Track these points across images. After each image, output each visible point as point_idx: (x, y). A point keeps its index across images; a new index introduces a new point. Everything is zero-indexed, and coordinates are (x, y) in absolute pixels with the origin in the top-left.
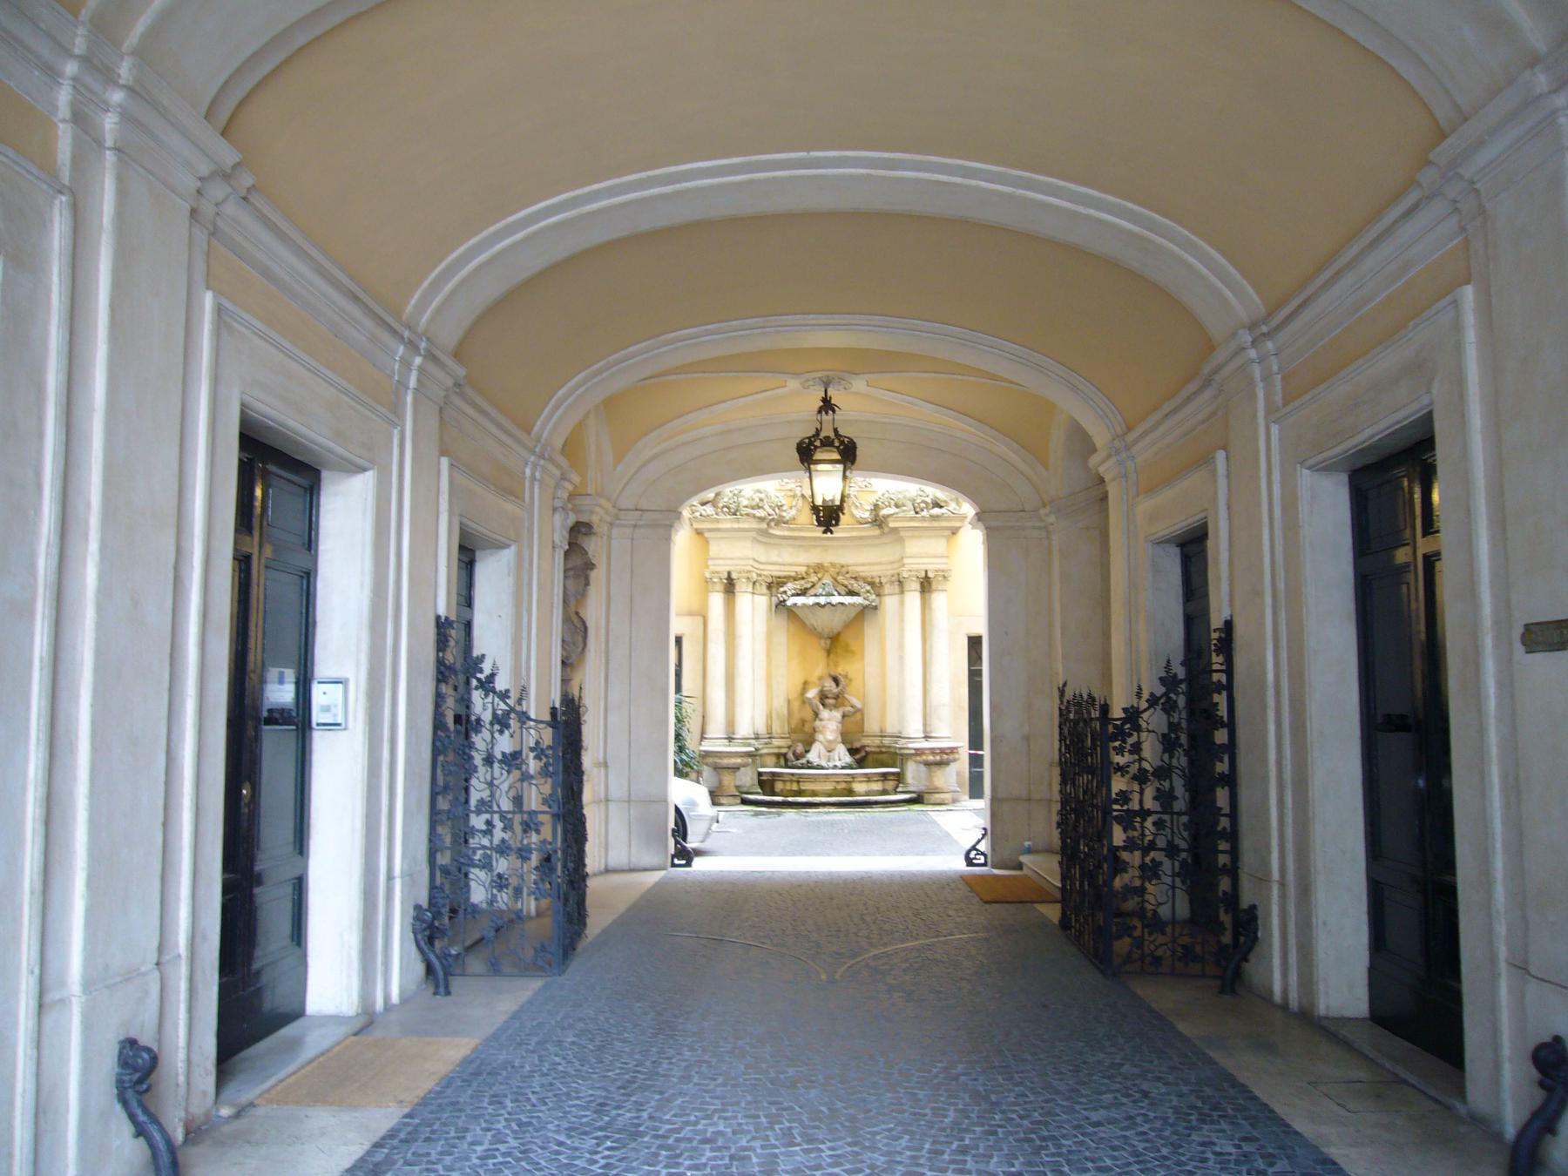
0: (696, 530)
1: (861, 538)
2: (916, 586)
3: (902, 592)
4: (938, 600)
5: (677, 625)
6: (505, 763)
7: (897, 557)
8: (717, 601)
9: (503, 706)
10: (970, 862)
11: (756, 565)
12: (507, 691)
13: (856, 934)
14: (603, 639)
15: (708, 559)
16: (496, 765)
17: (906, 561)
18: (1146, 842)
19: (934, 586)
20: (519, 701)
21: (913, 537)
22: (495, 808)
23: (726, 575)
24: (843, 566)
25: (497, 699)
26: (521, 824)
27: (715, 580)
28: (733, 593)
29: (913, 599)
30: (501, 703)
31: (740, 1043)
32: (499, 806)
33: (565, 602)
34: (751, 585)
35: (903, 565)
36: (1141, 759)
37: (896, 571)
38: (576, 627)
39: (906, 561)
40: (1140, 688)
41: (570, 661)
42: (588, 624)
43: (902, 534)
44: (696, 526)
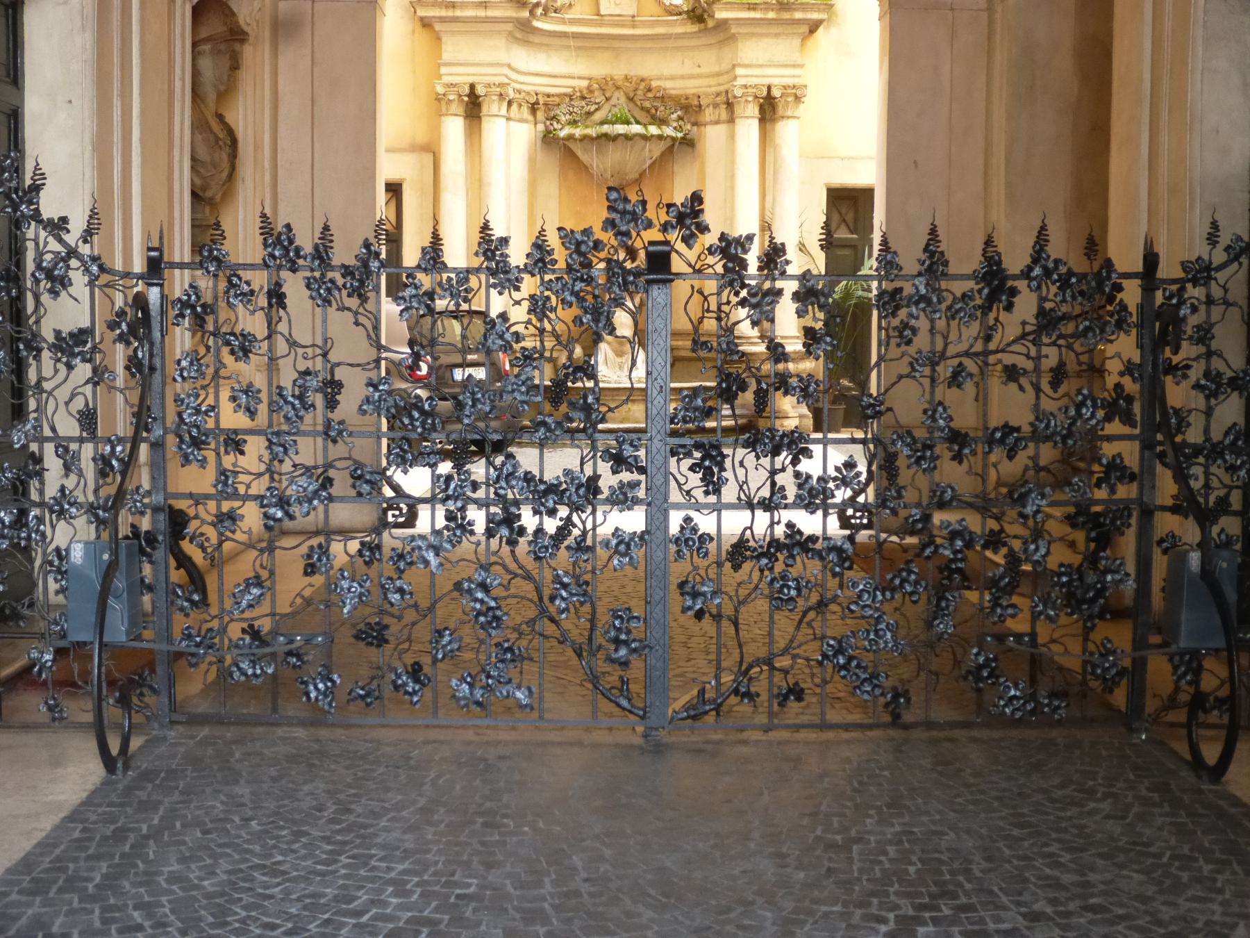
0: (422, 19)
1: (668, 37)
2: (753, 110)
3: (731, 120)
4: (787, 131)
5: (388, 167)
6: (63, 352)
7: (725, 66)
8: (454, 128)
9: (54, 245)
10: (295, 441)
11: (514, 76)
12: (64, 220)
13: (685, 645)
14: (267, 164)
15: (439, 65)
16: (46, 355)
17: (739, 71)
18: (1212, 499)
19: (780, 111)
20: (87, 236)
21: (752, 35)
22: (47, 432)
23: (467, 91)
24: (642, 80)
25: (43, 234)
26: (94, 459)
27: (451, 97)
28: (479, 118)
29: (748, 128)
30: (50, 239)
31: (494, 877)
32: (53, 429)
33: (197, 95)
34: (505, 104)
35: (735, 78)
36: (1209, 354)
37: (722, 88)
38: (217, 139)
39: (739, 71)
40: (1215, 225)
41: (209, 194)
42: (240, 136)
43: (734, 30)
44: (422, 12)
